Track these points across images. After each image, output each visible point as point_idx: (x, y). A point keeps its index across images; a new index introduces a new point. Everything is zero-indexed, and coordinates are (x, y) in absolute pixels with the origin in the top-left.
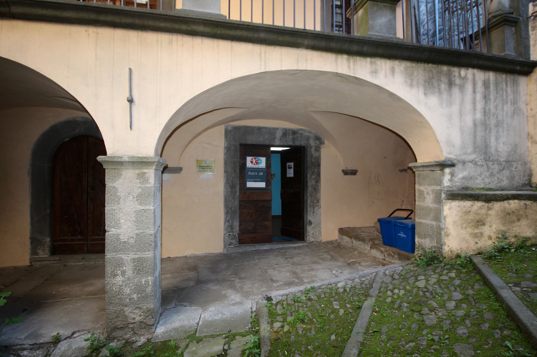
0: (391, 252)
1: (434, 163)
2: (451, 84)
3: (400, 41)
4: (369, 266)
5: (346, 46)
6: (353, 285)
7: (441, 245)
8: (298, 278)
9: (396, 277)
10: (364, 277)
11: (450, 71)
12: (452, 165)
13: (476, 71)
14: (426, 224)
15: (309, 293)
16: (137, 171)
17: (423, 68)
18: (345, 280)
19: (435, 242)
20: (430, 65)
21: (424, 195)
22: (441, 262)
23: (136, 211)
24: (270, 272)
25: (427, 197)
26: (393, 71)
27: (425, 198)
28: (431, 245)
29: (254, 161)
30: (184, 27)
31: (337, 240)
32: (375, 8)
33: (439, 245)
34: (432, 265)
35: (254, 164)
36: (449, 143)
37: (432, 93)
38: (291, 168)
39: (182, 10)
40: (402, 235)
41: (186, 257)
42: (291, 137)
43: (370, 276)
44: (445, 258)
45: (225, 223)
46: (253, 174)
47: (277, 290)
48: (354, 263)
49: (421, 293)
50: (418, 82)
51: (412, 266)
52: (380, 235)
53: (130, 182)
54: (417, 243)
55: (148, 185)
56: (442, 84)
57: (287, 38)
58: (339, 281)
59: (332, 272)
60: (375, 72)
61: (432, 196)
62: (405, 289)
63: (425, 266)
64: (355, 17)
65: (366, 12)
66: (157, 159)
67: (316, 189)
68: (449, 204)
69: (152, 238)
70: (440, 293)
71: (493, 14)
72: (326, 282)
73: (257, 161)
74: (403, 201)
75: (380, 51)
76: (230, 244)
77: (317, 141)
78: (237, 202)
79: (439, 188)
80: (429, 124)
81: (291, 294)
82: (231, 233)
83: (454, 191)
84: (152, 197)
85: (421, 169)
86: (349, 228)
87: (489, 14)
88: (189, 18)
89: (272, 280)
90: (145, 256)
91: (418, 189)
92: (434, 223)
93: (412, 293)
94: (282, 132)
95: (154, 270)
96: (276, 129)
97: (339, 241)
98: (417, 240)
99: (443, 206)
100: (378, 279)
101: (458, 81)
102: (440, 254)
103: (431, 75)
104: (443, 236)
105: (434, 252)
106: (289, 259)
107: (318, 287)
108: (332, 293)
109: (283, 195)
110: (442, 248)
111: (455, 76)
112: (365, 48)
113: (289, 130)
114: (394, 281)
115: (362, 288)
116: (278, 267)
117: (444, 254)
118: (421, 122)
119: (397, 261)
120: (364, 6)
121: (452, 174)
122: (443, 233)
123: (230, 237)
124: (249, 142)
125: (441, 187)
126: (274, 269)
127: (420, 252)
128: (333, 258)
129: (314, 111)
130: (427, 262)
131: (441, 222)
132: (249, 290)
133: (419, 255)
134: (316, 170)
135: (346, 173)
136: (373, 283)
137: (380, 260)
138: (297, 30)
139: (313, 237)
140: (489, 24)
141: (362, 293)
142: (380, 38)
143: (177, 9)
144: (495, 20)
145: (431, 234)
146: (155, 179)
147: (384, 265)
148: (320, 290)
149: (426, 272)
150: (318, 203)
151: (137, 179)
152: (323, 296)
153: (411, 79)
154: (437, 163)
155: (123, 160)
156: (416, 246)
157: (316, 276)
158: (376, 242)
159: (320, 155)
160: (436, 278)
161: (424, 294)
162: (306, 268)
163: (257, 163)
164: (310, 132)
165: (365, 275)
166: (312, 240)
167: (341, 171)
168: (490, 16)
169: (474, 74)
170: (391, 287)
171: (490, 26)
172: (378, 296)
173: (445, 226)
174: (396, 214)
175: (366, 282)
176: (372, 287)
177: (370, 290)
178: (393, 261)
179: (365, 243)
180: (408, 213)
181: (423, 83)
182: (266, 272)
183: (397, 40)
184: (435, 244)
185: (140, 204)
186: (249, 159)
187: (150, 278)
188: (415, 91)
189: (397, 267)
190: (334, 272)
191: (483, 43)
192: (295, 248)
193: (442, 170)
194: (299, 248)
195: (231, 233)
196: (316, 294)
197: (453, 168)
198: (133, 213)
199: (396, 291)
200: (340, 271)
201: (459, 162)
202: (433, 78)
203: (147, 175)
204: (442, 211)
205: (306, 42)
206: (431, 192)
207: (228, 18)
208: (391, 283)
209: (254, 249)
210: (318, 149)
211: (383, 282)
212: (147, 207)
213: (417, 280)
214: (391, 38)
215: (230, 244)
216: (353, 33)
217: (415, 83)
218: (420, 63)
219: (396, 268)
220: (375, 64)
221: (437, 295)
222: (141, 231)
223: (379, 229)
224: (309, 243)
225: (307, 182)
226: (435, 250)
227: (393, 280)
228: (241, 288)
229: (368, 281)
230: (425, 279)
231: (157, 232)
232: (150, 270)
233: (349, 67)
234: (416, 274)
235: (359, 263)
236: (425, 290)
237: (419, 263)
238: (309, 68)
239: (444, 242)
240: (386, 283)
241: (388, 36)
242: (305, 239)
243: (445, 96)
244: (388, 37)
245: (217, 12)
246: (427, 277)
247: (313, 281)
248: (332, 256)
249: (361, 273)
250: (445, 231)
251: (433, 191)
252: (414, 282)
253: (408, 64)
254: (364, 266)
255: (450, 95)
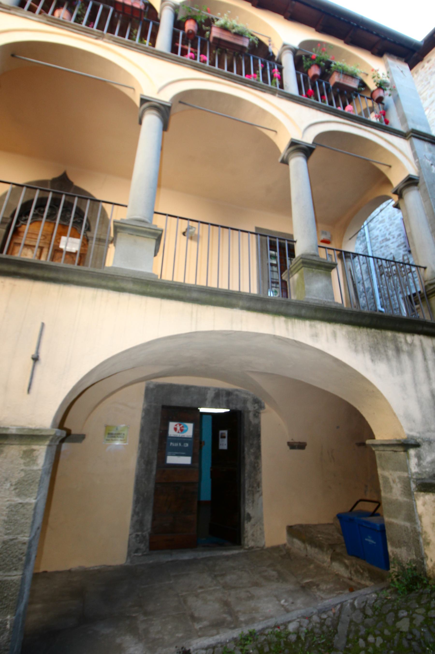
0: (358, 567)
1: (395, 442)
2: (398, 350)
3: (339, 306)
4: (331, 591)
5: (283, 309)
6: (311, 626)
7: (423, 559)
8: (231, 613)
9: (369, 612)
10: (324, 612)
11: (395, 336)
12: (417, 445)
13: (422, 337)
14: (398, 525)
15: (246, 643)
16: (24, 448)
17: (366, 333)
18: (298, 618)
19: (414, 553)
20: (373, 330)
21: (389, 483)
22: (425, 586)
23: (11, 505)
24: (192, 601)
25: (394, 486)
26: (334, 334)
27: (391, 488)
28: (409, 558)
29: (178, 428)
30: (111, 284)
31: (285, 545)
32: (311, 274)
33: (419, 559)
34: (414, 590)
35: (178, 432)
36: (408, 417)
37: (379, 360)
38: (224, 437)
39: (112, 267)
40: (370, 540)
41: (70, 571)
42: (225, 399)
43: (333, 611)
44: (430, 579)
45: (133, 516)
46: (176, 445)
47: (200, 636)
48: (309, 585)
49: (405, 643)
50: (362, 348)
51: (389, 591)
52: (342, 538)
53: (12, 462)
54: (390, 554)
55: (35, 468)
56: (389, 351)
57: (221, 299)
58: (290, 619)
59: (280, 601)
60: (315, 336)
61: (399, 486)
62: (382, 635)
63: (406, 593)
64: (291, 280)
65: (301, 276)
66: (55, 431)
67: (256, 468)
68: (422, 498)
69: (25, 547)
70: (431, 642)
71: (429, 282)
72: (271, 622)
73: (182, 428)
74: (366, 486)
75: (319, 315)
76: (137, 551)
77: (256, 405)
78: (152, 485)
79: (405, 475)
80: (381, 394)
81: (219, 645)
82: (139, 533)
83: (425, 479)
84: (37, 485)
85: (381, 448)
86: (301, 526)
87: (425, 281)
88: (118, 276)
89: (194, 618)
90: (9, 578)
91: (381, 475)
92: (408, 524)
93: (393, 643)
94: (214, 392)
95: (18, 603)
96: (207, 389)
97: (288, 545)
98: (390, 549)
99: (415, 501)
100: (344, 617)
101: (405, 347)
102: (422, 573)
103: (376, 340)
104: (422, 545)
105: (415, 569)
106: (219, 578)
107: (259, 631)
108: (280, 642)
109: (214, 474)
110: (423, 563)
111: (401, 342)
112: (303, 312)
113: (223, 390)
114: (368, 620)
115: (323, 632)
116: (202, 593)
117: (428, 572)
118: (373, 392)
119: (368, 583)
120: (300, 272)
121: (419, 457)
122: (421, 540)
123: (138, 539)
124: (174, 404)
125: (409, 474)
126: (197, 596)
127: (397, 568)
128: (281, 578)
129: (252, 372)
130: (407, 586)
131: (416, 523)
132: (157, 637)
133: (396, 574)
134: (255, 442)
135: (292, 446)
136: (338, 624)
137: (345, 580)
138: (231, 292)
139: (253, 540)
140: (427, 290)
141: (323, 643)
142: (317, 302)
143: (106, 267)
144: (432, 287)
145: (406, 541)
146: (46, 460)
147: (352, 590)
148: (263, 638)
149: (409, 603)
150: (259, 487)
151: (22, 458)
152: (266, 649)
153: (355, 344)
154: (399, 443)
155: (8, 432)
156: (391, 560)
157: (256, 610)
158: (338, 550)
159: (259, 422)
160: (423, 615)
161: (410, 644)
162: (243, 594)
163: (182, 430)
164: (247, 394)
165: (326, 608)
166: (251, 544)
167: (286, 444)
168: (426, 284)
169: (421, 341)
170: (363, 631)
171: (428, 293)
172: (345, 648)
173: (422, 529)
174: (362, 506)
175: (328, 622)
176: (337, 632)
177: (334, 636)
178: (363, 582)
179: (323, 551)
180: (374, 506)
181: (369, 348)
182: (185, 602)
183: (335, 305)
184: (414, 557)
185: (19, 495)
186: (172, 425)
187: (9, 617)
188: (360, 357)
189: (369, 594)
190: (282, 602)
191: (424, 309)
192: (227, 558)
193: (406, 451)
194: (233, 557)
195: (139, 533)
196: (257, 646)
197: (418, 449)
198: (5, 508)
199: (371, 639)
200: (291, 600)
201: (424, 441)
202: (378, 343)
203: (36, 453)
204: (415, 507)
205: (241, 303)
206: (397, 480)
207: (159, 277)
208: (363, 623)
209: (170, 559)
210: (257, 414)
211: (351, 621)
212: (27, 500)
213: (398, 619)
214: (328, 302)
215: (137, 551)
216: (290, 297)
217: (359, 348)
218: (362, 327)
219: (368, 596)
220: (315, 327)
221: (428, 646)
222: (11, 537)
223: (340, 528)
224: (247, 549)
225: (244, 458)
226: (416, 567)
227: (365, 618)
228: (146, 631)
229: (330, 619)
230: (408, 616)
231: (34, 537)
232: (11, 603)
233: (287, 330)
234: (395, 607)
235: (318, 585)
236: (410, 637)
237: (397, 587)
238: (244, 329)
239: (425, 554)
240: (356, 625)
241: (326, 300)
242: (242, 543)
243: (394, 363)
244: (326, 301)
245: (149, 271)
246: (411, 612)
247: (252, 620)
248: (279, 573)
249: (320, 605)
250: (424, 536)
251: (399, 478)
252: (395, 622)
253: (350, 328)
254: (324, 591)
255: (399, 361)
